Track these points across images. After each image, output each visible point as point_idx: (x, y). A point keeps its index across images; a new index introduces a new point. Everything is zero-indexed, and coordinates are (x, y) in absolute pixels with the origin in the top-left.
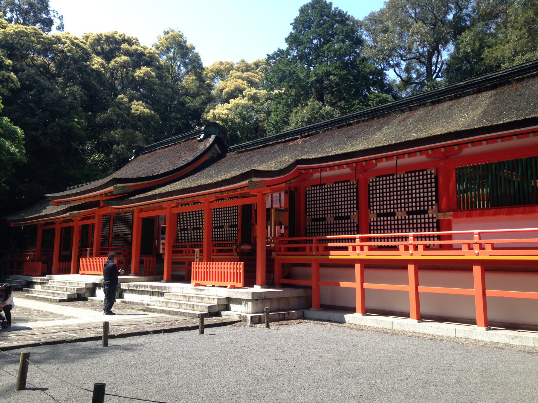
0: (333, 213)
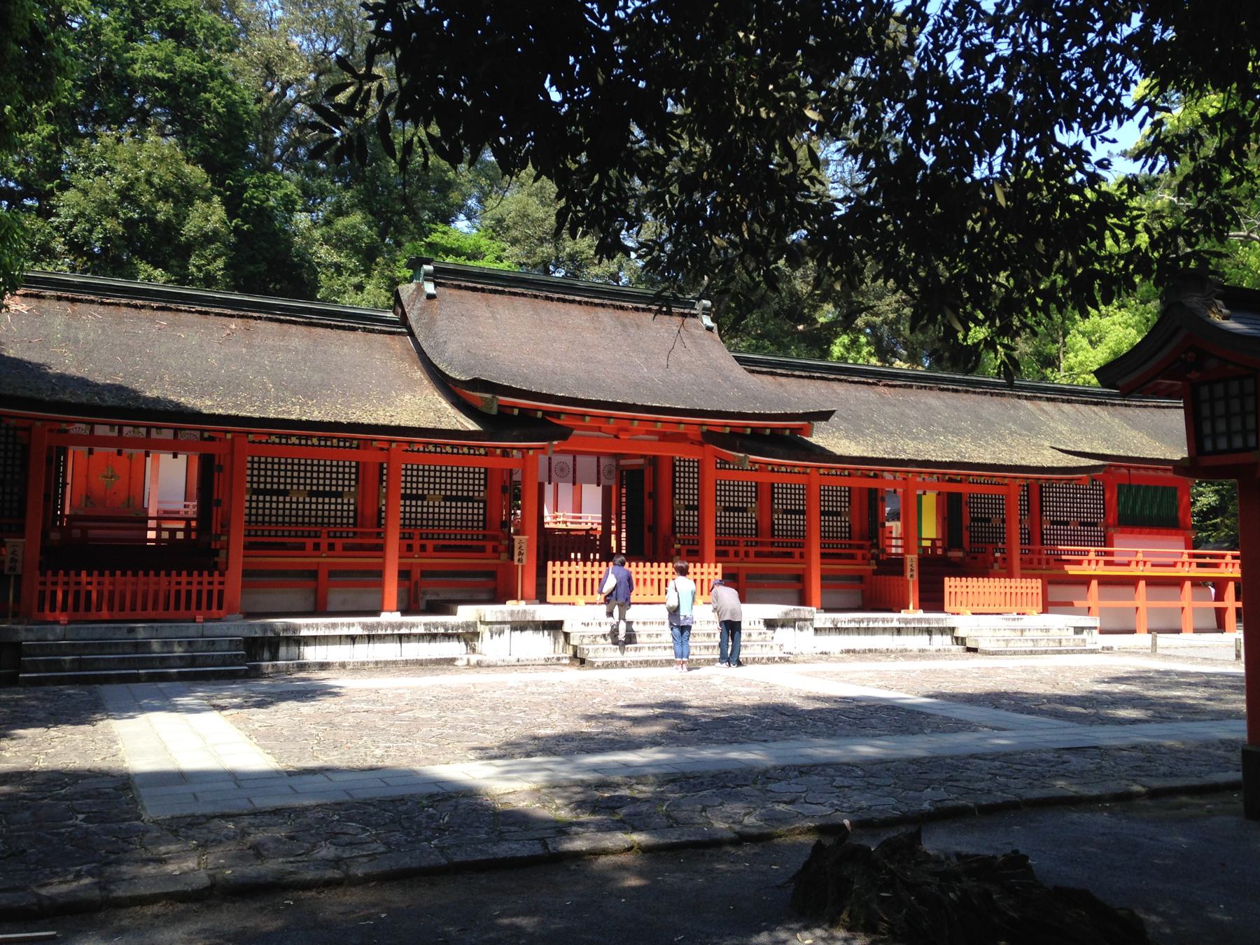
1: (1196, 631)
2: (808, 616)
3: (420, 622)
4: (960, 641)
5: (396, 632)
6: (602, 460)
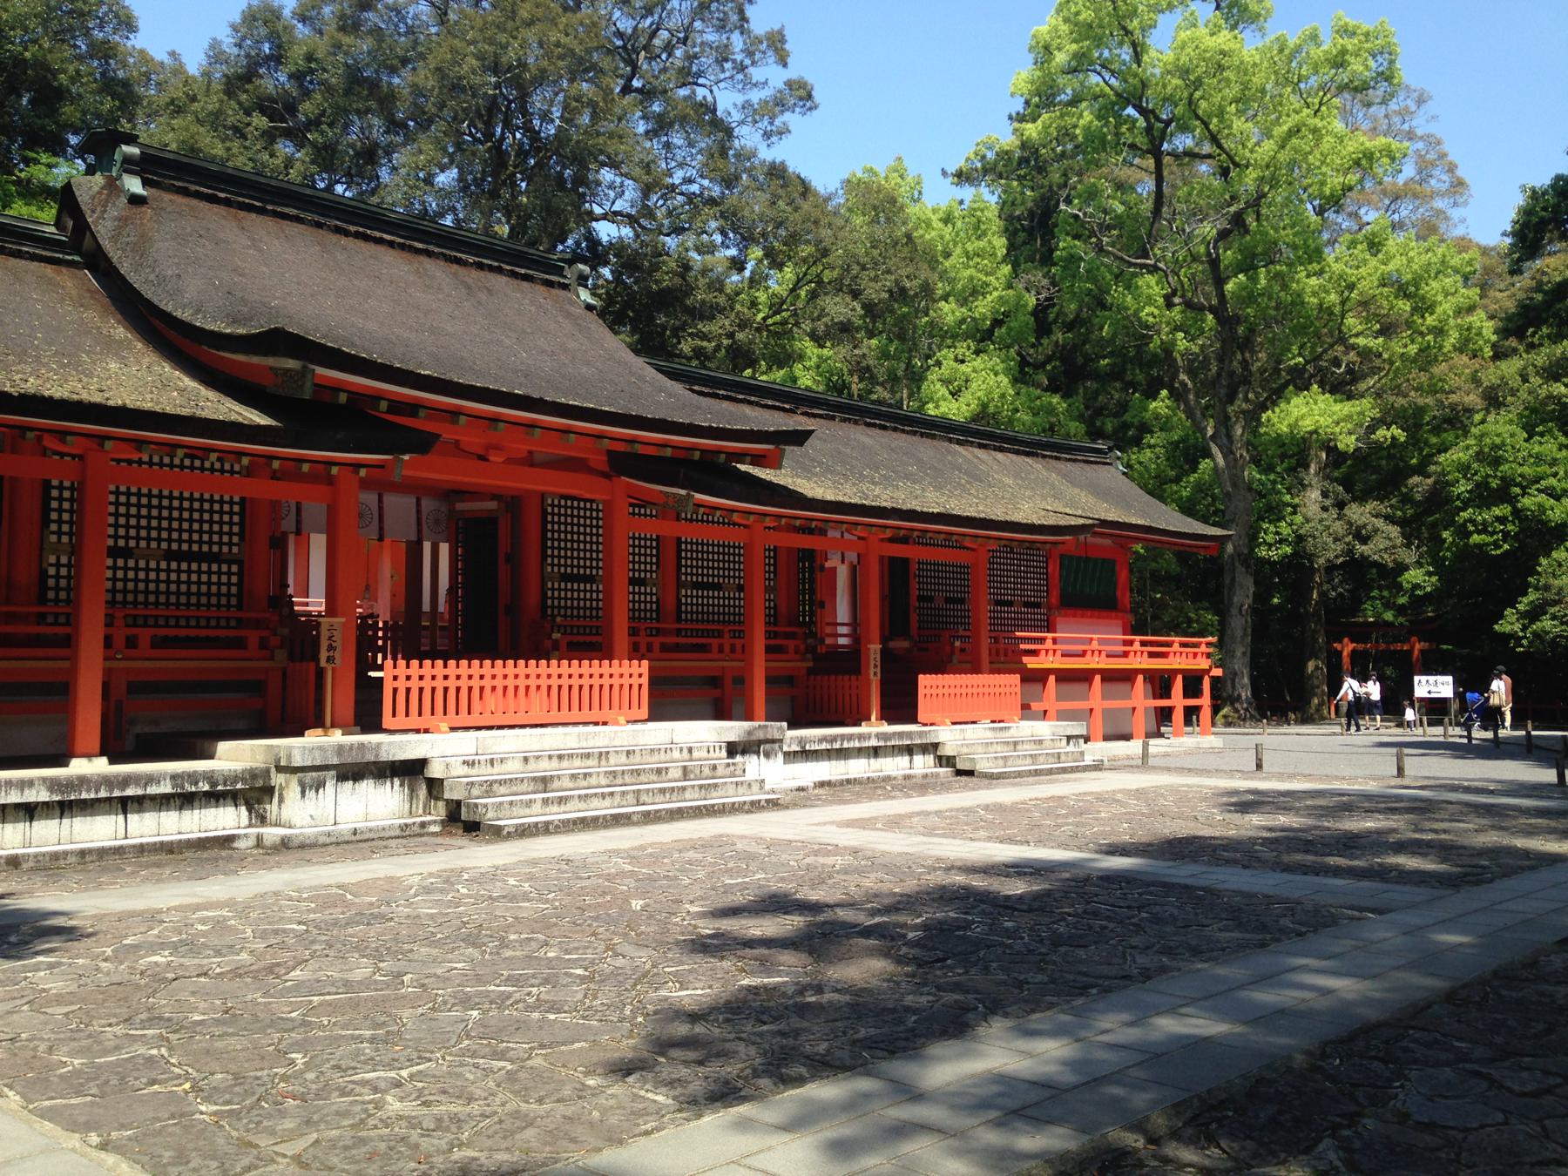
0: (559, 565)
1: (1106, 738)
2: (777, 736)
3: (164, 771)
4: (947, 761)
5: (117, 793)
6: (424, 502)
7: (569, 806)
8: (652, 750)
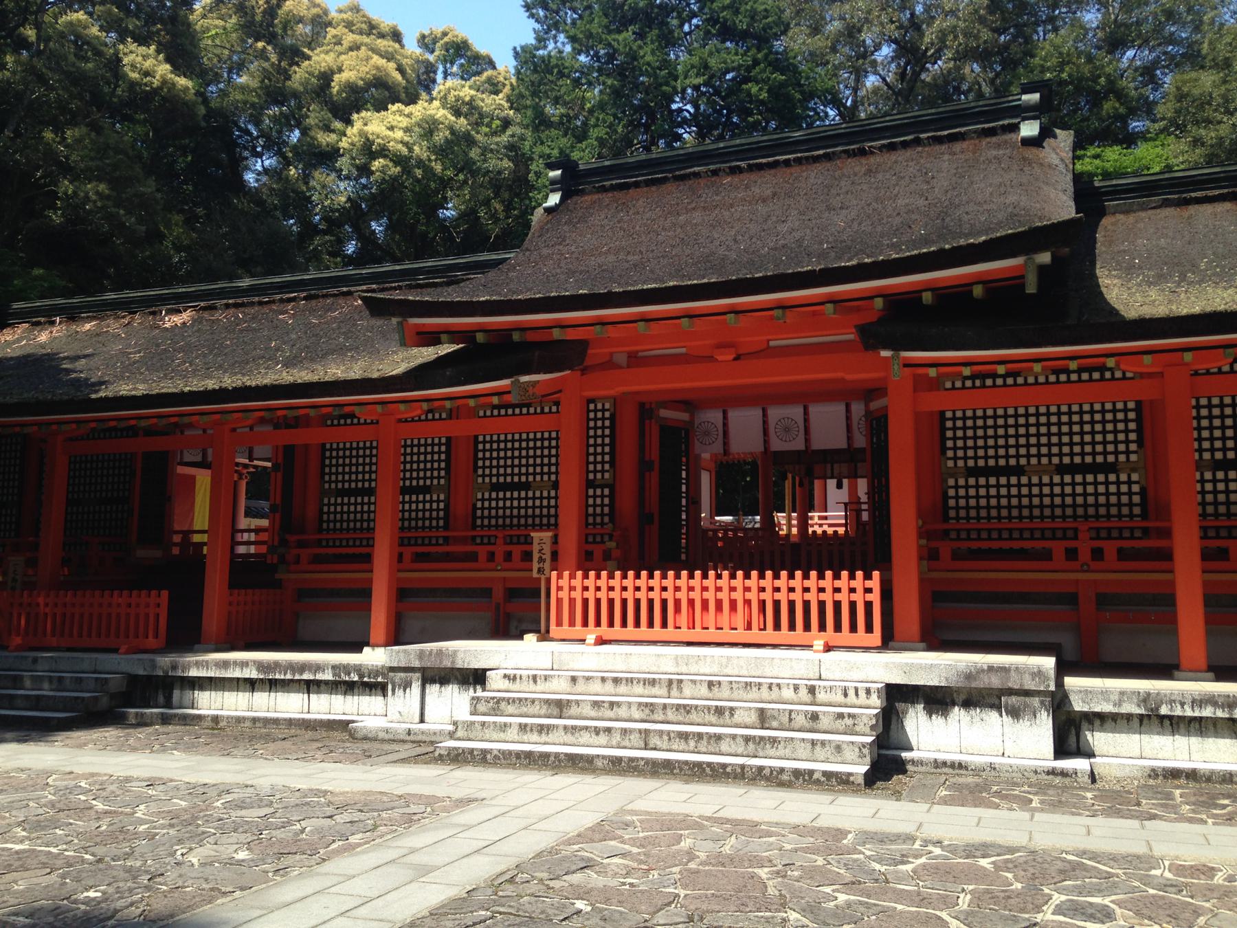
7: (552, 737)
8: (748, 685)
